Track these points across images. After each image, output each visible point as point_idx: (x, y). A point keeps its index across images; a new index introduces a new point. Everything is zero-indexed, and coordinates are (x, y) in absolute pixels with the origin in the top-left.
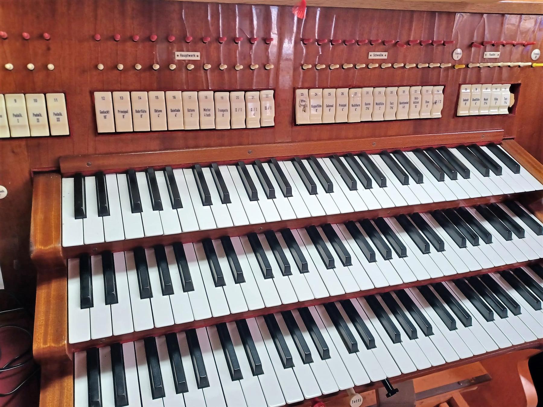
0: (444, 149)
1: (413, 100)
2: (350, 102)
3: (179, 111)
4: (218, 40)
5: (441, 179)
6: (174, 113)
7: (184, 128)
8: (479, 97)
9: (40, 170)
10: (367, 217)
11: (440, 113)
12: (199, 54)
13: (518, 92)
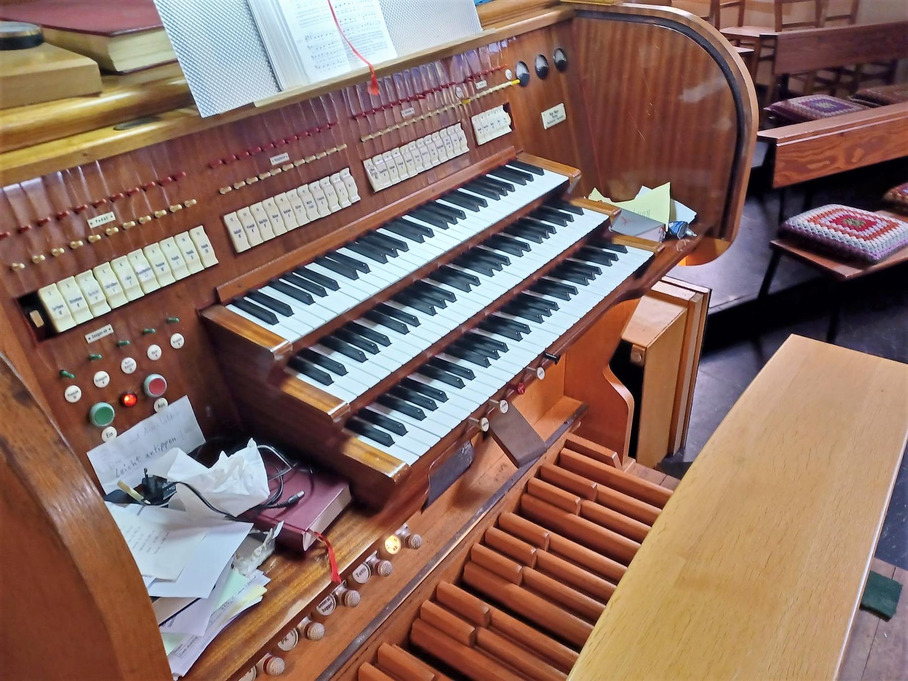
0: (300, 269)
1: (445, 142)
2: (326, 193)
3: (290, 211)
4: (77, 211)
6: (287, 214)
7: (298, 223)
8: (487, 124)
10: (326, 333)
11: (358, 196)
12: (286, 154)
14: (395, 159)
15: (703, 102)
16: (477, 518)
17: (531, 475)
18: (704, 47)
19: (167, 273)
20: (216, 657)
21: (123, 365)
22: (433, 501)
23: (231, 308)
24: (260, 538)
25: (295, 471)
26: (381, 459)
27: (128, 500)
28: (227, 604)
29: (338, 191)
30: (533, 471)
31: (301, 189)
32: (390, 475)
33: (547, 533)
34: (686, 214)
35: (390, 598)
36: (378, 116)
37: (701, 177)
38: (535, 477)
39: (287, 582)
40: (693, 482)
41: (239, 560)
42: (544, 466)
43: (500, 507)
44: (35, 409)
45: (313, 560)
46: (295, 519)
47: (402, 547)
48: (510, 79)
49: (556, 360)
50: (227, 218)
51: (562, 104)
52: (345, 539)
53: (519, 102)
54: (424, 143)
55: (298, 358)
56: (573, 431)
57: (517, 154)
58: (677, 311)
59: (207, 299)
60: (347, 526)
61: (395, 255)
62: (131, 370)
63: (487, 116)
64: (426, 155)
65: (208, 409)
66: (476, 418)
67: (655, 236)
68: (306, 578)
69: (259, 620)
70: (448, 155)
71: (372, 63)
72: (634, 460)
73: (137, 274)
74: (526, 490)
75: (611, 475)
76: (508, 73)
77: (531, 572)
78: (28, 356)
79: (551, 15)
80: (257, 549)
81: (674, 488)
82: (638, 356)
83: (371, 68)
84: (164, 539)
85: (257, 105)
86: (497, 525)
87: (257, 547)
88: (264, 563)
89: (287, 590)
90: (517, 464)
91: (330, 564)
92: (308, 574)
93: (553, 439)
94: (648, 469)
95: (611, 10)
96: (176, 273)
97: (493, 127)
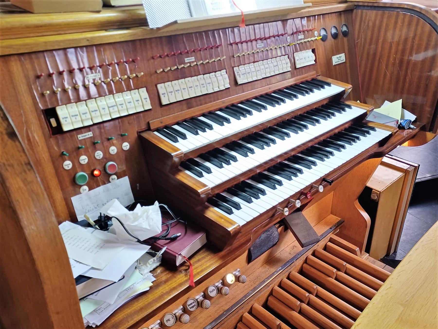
5: (197, 134)
6: (191, 88)
8: (302, 58)
9: (141, 130)
12: (193, 58)
13: (315, 52)
14: (251, 69)
15: (424, 61)
16: (277, 272)
17: (309, 253)
18: (428, 23)
19: (124, 110)
20: (118, 318)
21: (96, 154)
22: (255, 259)
23: (156, 133)
24: (153, 255)
25: (178, 223)
26: (225, 220)
27: (89, 225)
28: (129, 288)
29: (219, 81)
30: (310, 252)
31: (199, 77)
32: (229, 230)
33: (315, 286)
34: (412, 117)
35: (226, 308)
36: (244, 45)
37: (420, 99)
38: (311, 255)
39: (166, 281)
40: (409, 262)
41: (140, 265)
42: (317, 249)
43: (291, 268)
44: (17, 143)
45: (181, 272)
46: (173, 247)
47: (236, 281)
48: (317, 36)
49: (330, 183)
50: (159, 86)
51: (344, 54)
52: (200, 263)
53: (320, 51)
54: (267, 63)
55: (187, 163)
56: (334, 233)
57: (317, 76)
58: (398, 175)
59: (144, 127)
60: (202, 256)
61: (246, 117)
62: (100, 157)
63: (303, 54)
64: (268, 69)
65: (138, 185)
66: (281, 208)
67: (393, 124)
68: (175, 281)
69: (146, 301)
70: (280, 71)
71: (243, 11)
72: (368, 254)
73: (109, 107)
74: (306, 261)
75: (355, 260)
76: (316, 33)
77: (305, 306)
78: (46, 141)
79: (342, 6)
80: (150, 260)
81: (391, 272)
82: (375, 196)
83: (242, 13)
84: (101, 247)
85: (179, 22)
86: (288, 278)
87: (151, 259)
88: (154, 269)
89: (164, 286)
90: (302, 246)
91: (190, 275)
92: (177, 279)
93: (323, 236)
94: (375, 260)
95: (376, 5)
96: (129, 110)
97: (305, 60)
